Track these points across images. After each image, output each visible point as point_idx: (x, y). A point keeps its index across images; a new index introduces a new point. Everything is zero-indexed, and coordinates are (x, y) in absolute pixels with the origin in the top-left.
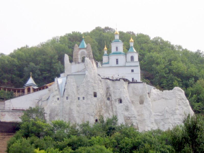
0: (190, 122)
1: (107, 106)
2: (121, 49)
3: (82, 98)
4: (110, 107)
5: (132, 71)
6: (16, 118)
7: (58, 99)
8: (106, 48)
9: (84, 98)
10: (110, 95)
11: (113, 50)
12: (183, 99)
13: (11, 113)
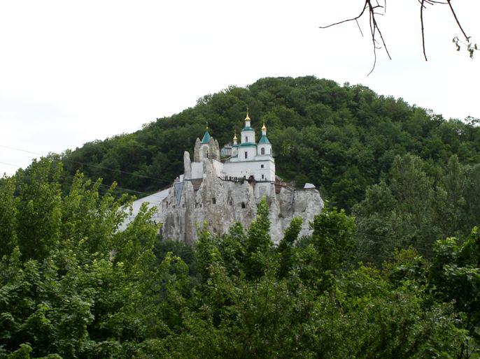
0: (462, 271)
1: (227, 212)
2: (252, 138)
4: (232, 214)
5: (262, 166)
8: (235, 138)
10: (232, 199)
11: (243, 141)
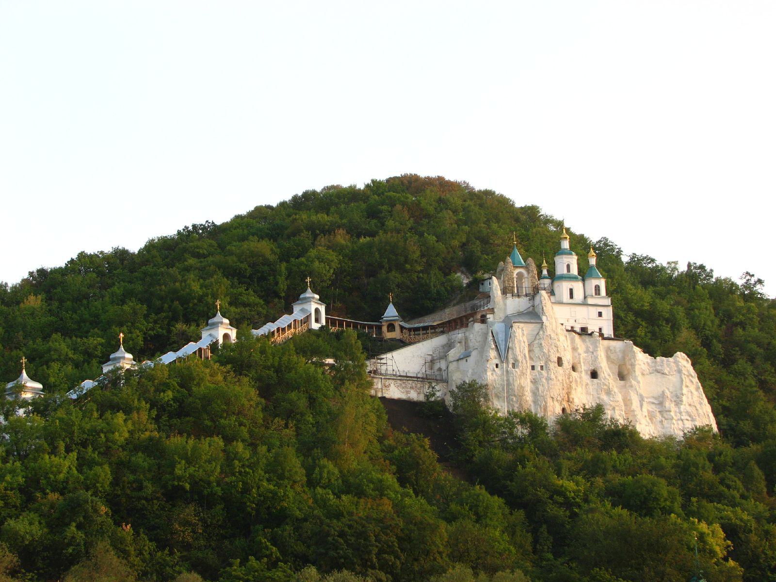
2: (574, 271)
3: (539, 368)
5: (600, 314)
6: (408, 392)
7: (497, 366)
9: (542, 367)
11: (561, 270)
12: (692, 376)
13: (399, 382)
